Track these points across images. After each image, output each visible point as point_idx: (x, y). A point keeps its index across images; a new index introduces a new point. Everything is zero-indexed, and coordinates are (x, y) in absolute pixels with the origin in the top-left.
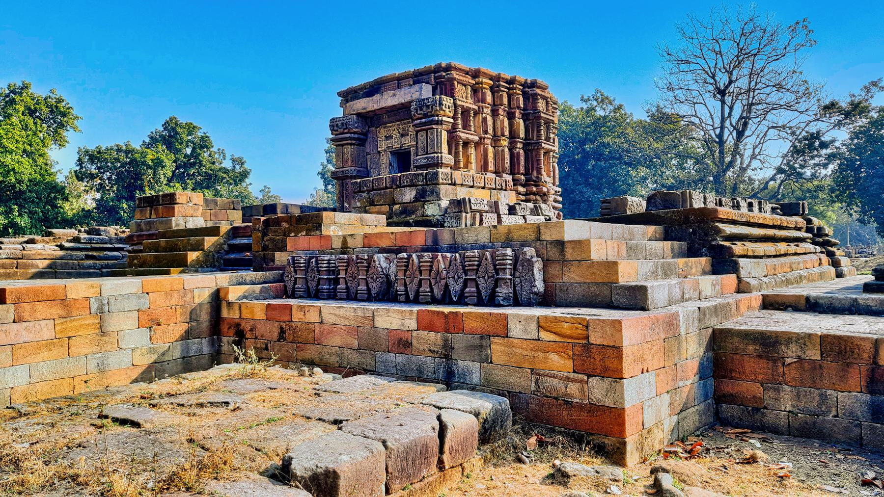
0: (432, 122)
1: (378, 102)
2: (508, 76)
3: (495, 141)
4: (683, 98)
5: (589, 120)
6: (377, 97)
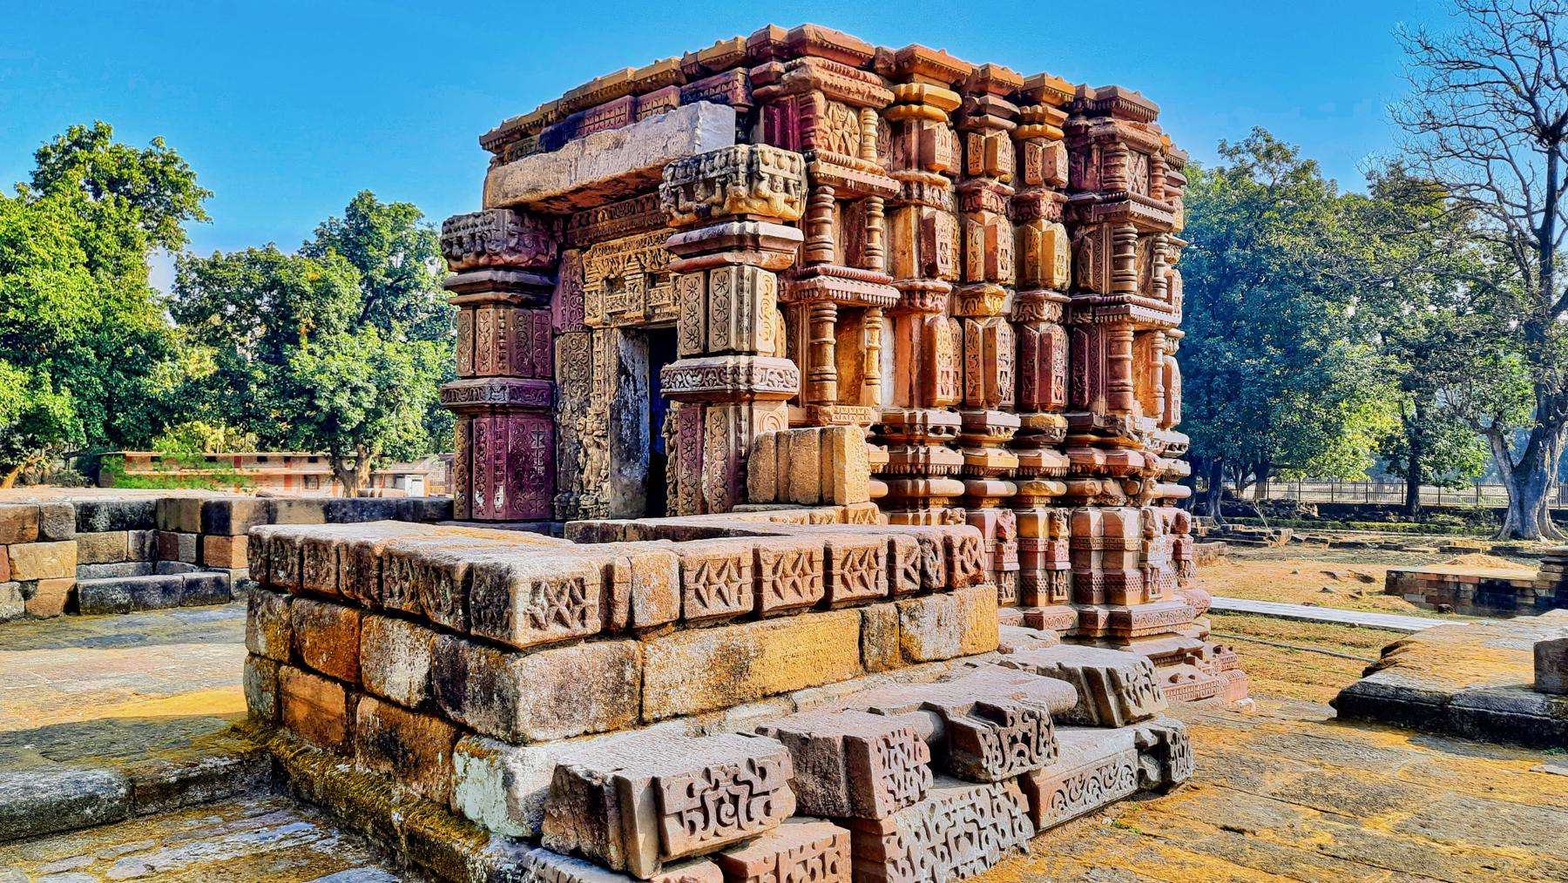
0: (722, 243)
1: (573, 165)
2: (1018, 76)
3: (963, 297)
4: (1457, 144)
5: (1233, 197)
6: (571, 148)
